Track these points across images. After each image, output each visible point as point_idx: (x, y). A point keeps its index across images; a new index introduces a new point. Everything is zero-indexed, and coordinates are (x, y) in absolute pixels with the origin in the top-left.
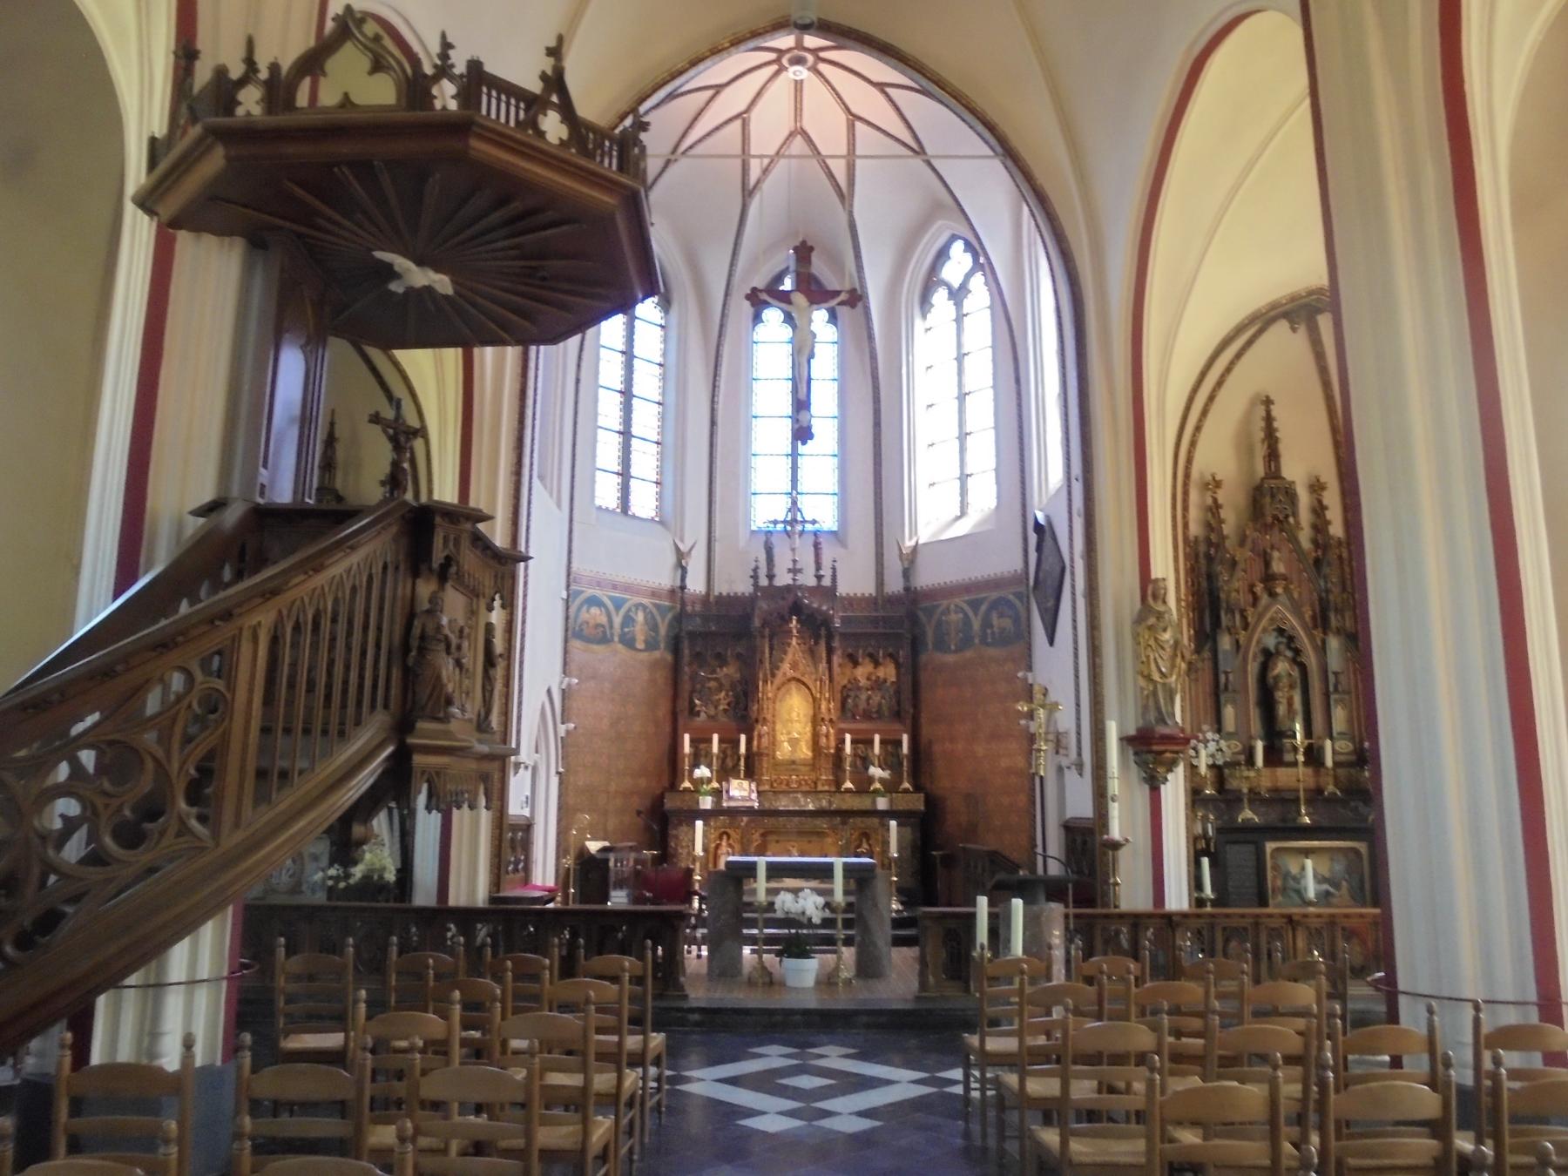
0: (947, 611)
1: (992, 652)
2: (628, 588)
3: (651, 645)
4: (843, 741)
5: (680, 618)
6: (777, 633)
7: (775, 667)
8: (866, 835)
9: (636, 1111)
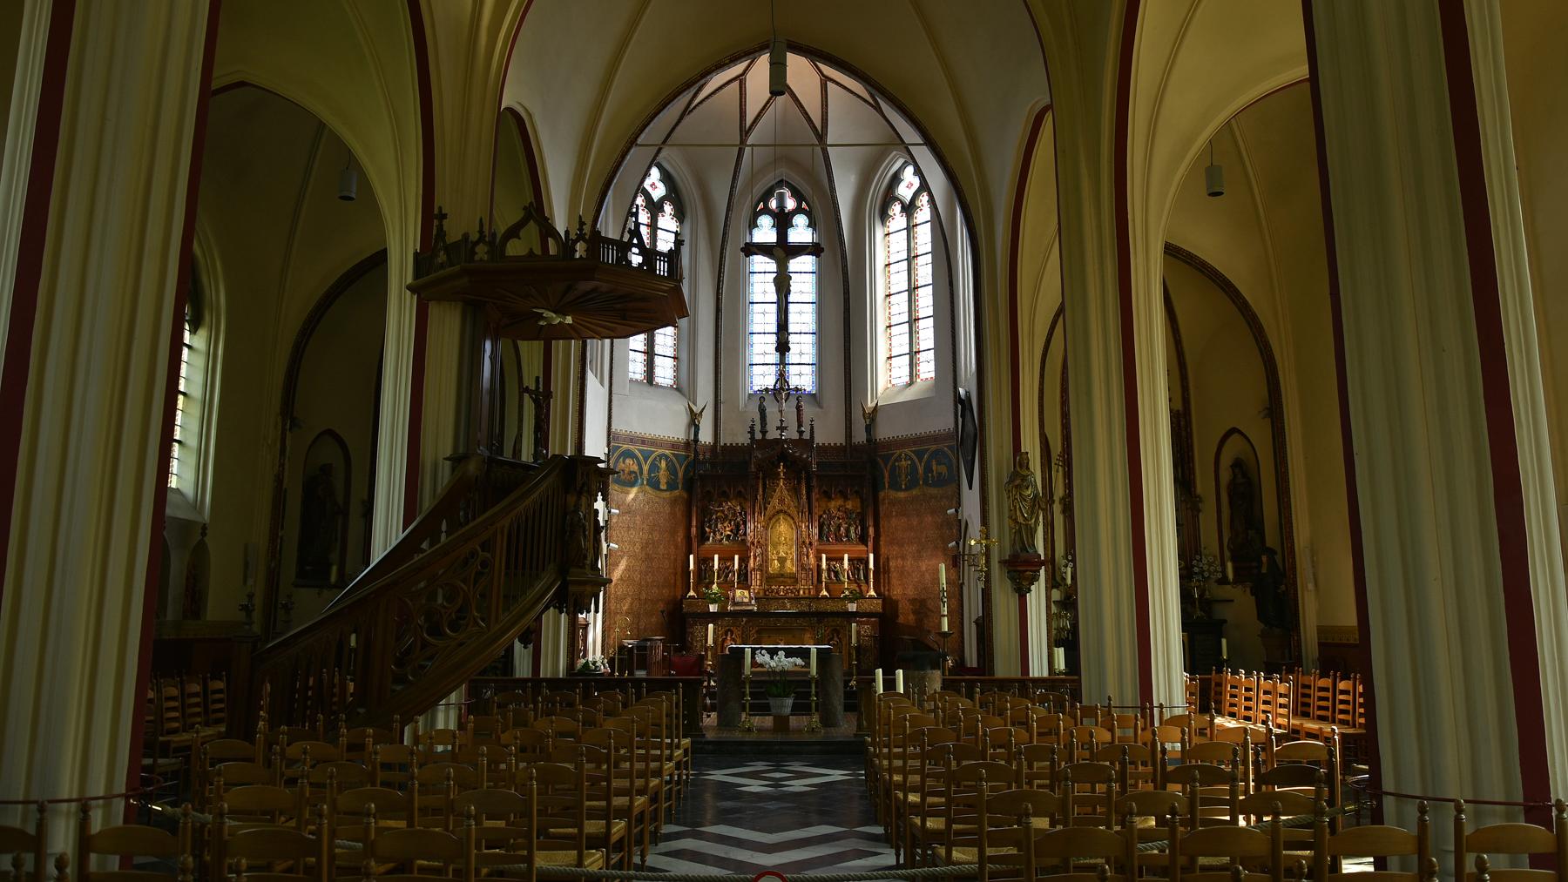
0: (899, 459)
1: (934, 491)
2: (654, 442)
3: (671, 486)
4: (820, 559)
5: (694, 464)
6: (770, 475)
7: (766, 502)
8: (836, 631)
9: (673, 802)
